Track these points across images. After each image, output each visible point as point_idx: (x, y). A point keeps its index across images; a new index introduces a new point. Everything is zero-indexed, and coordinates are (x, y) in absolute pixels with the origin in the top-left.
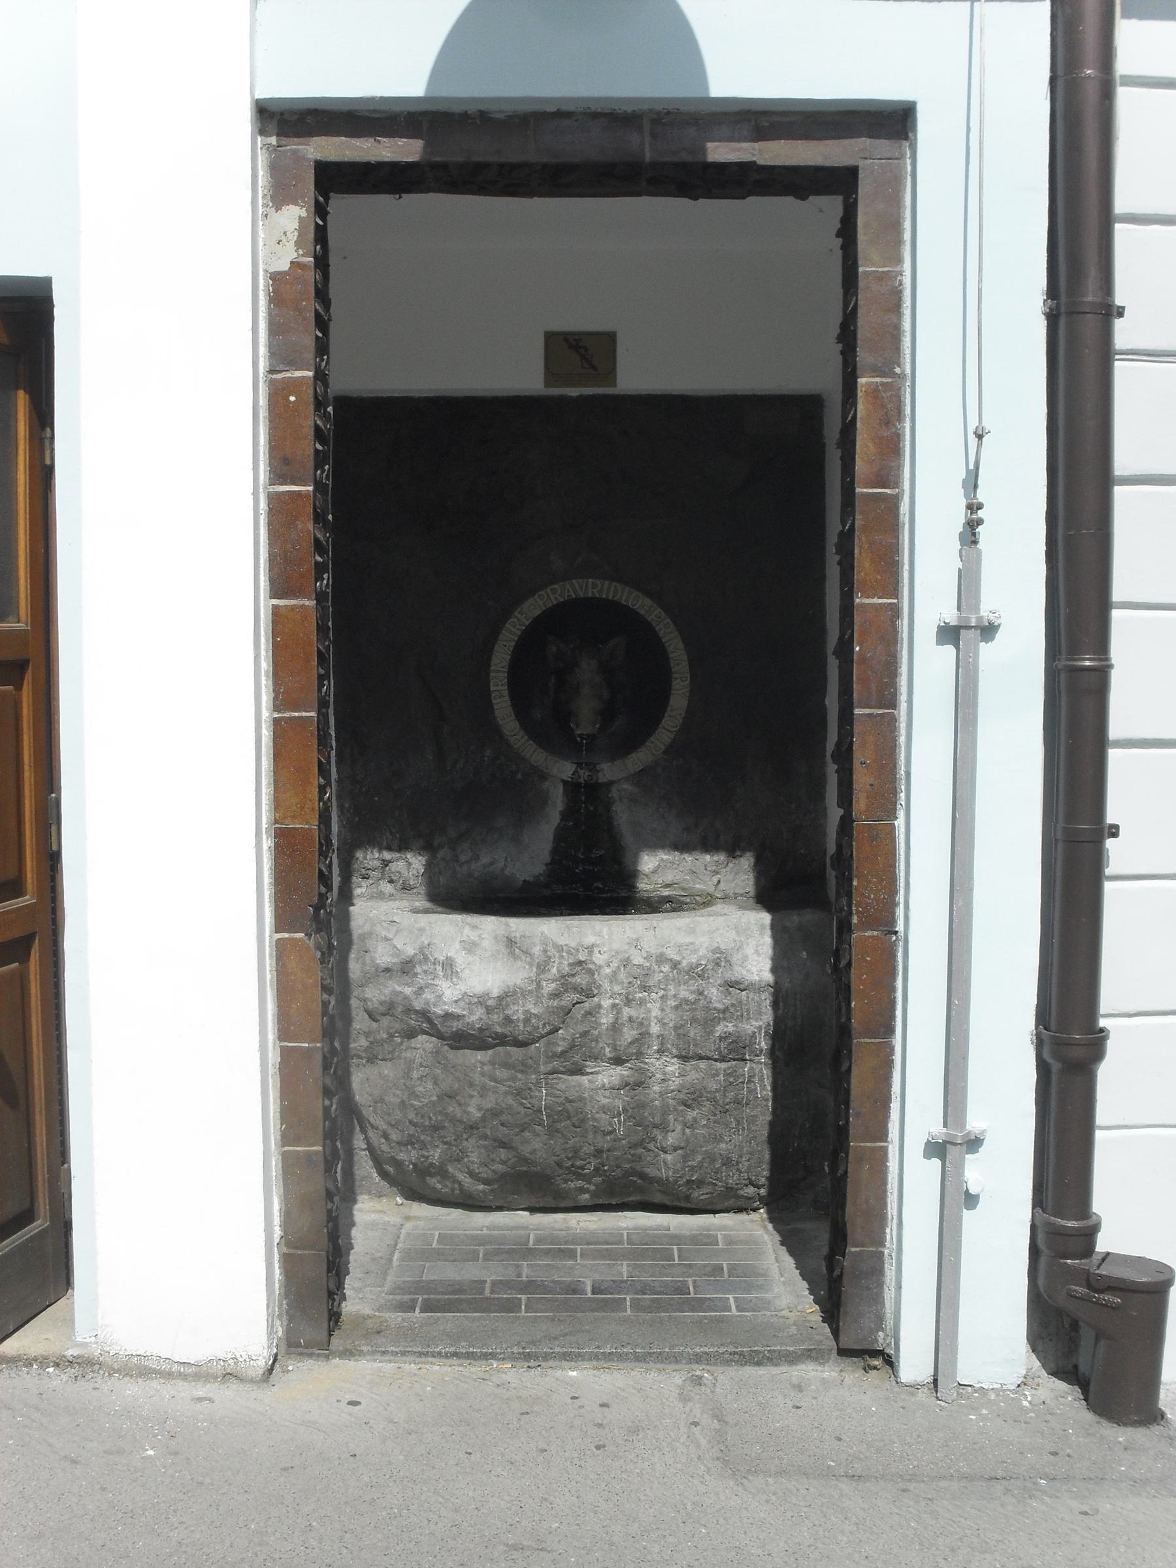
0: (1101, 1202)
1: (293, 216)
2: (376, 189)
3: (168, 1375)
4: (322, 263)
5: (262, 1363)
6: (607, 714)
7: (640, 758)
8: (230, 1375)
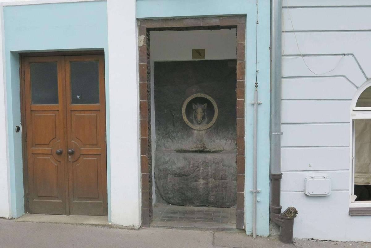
1: (143, 37)
2: (157, 30)
3: (123, 228)
4: (148, 44)
5: (138, 227)
6: (203, 118)
8: (132, 228)
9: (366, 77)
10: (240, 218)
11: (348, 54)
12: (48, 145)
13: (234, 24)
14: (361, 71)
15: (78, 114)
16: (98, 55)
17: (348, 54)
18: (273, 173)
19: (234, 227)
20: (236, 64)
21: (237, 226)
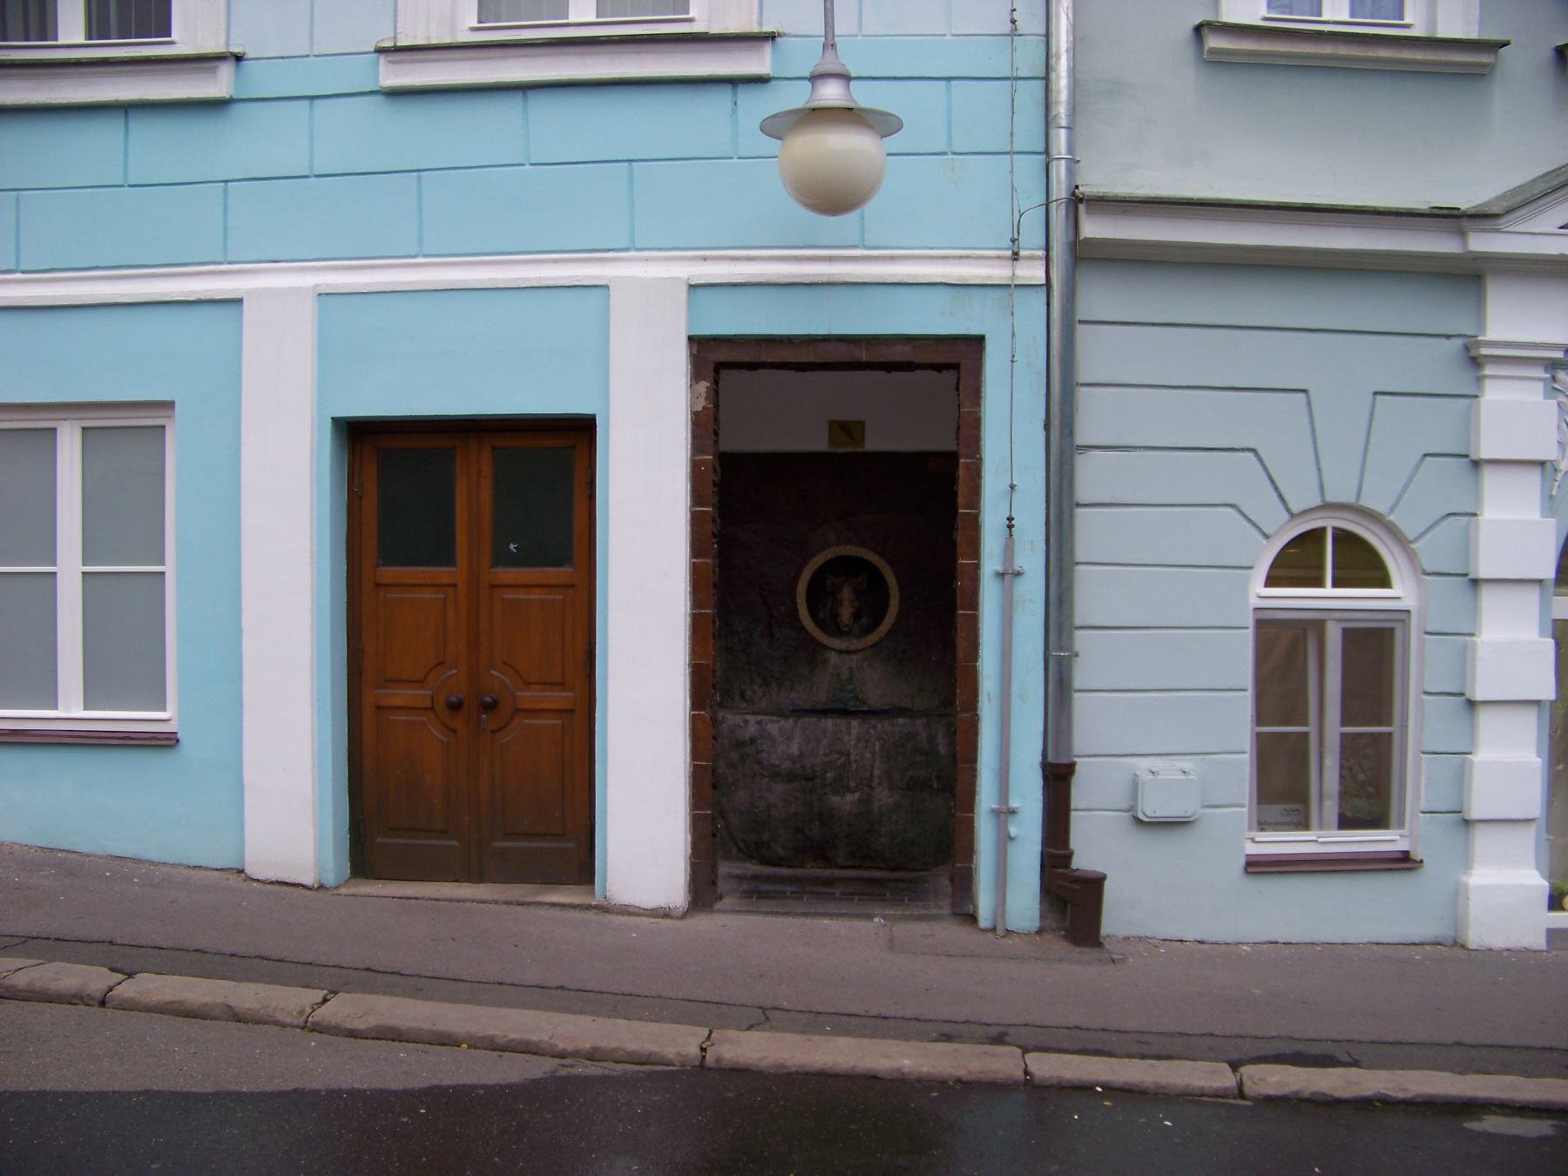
0: (1074, 843)
1: (703, 386)
3: (638, 915)
4: (716, 406)
6: (857, 616)
7: (873, 638)
8: (664, 913)
9: (1288, 510)
10: (964, 884)
11: (1243, 450)
12: (420, 683)
13: (952, 360)
14: (1275, 494)
15: (510, 595)
16: (577, 434)
17: (1243, 450)
18: (1051, 759)
19: (946, 910)
20: (957, 465)
21: (953, 905)
